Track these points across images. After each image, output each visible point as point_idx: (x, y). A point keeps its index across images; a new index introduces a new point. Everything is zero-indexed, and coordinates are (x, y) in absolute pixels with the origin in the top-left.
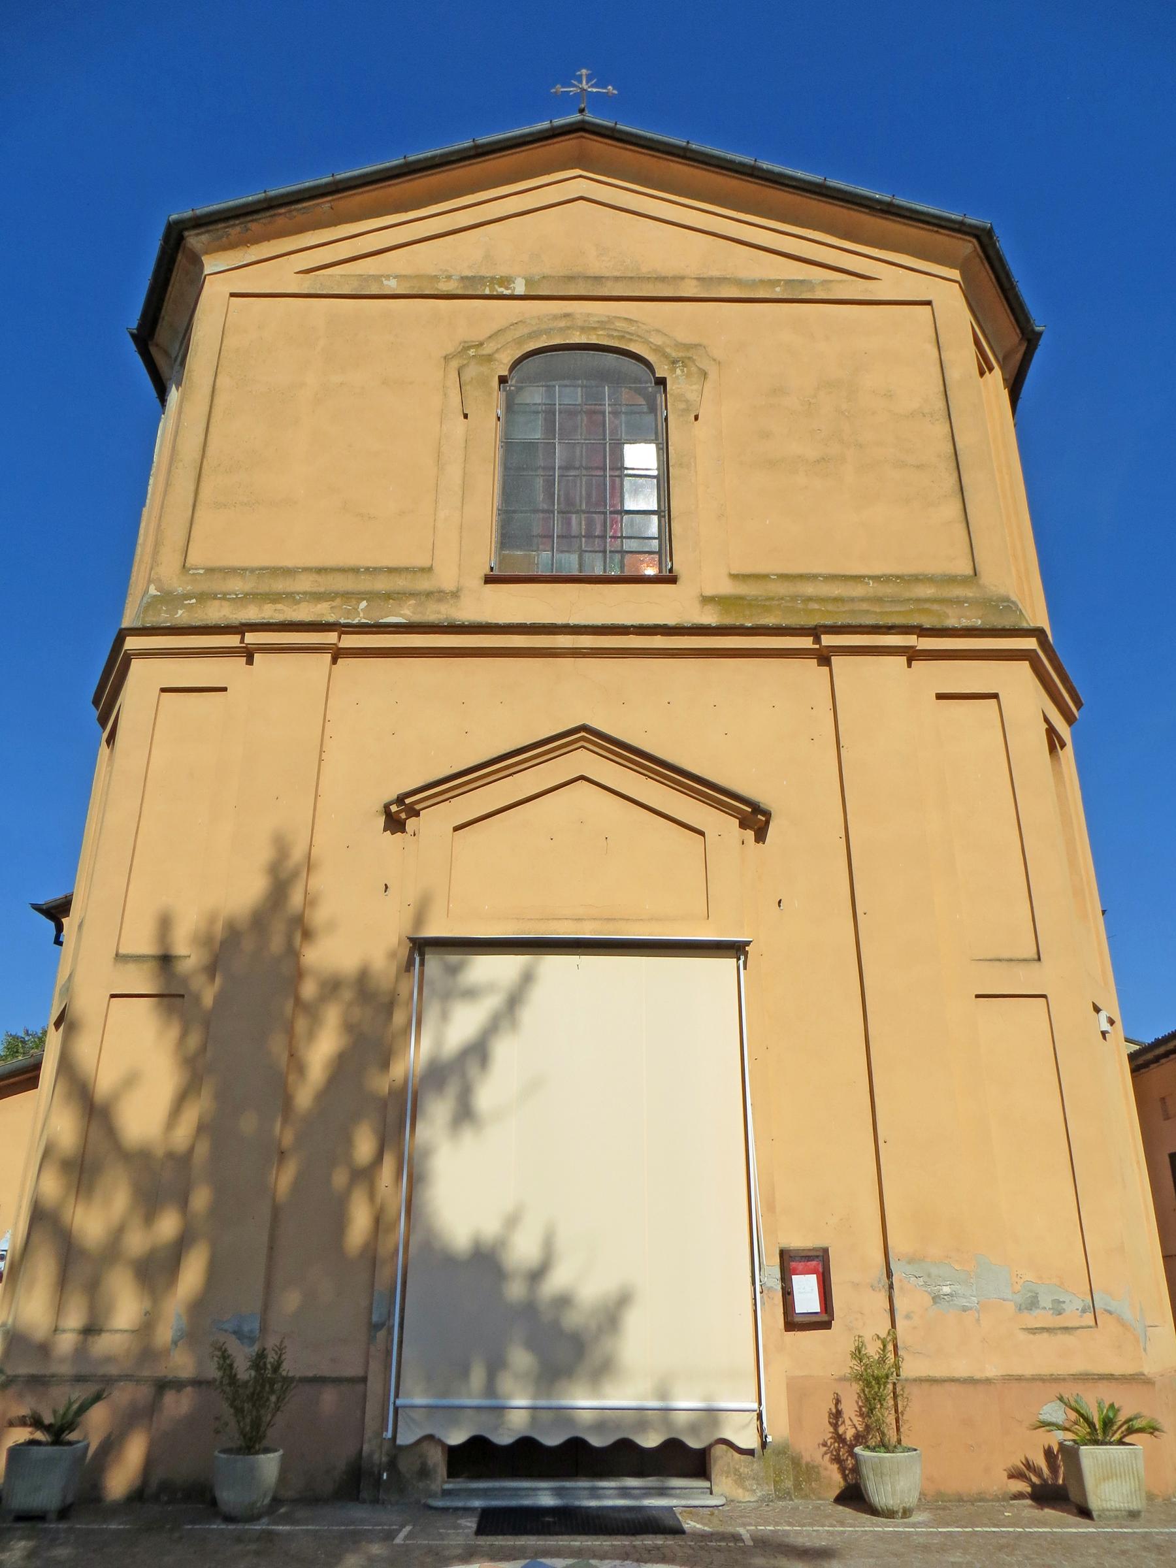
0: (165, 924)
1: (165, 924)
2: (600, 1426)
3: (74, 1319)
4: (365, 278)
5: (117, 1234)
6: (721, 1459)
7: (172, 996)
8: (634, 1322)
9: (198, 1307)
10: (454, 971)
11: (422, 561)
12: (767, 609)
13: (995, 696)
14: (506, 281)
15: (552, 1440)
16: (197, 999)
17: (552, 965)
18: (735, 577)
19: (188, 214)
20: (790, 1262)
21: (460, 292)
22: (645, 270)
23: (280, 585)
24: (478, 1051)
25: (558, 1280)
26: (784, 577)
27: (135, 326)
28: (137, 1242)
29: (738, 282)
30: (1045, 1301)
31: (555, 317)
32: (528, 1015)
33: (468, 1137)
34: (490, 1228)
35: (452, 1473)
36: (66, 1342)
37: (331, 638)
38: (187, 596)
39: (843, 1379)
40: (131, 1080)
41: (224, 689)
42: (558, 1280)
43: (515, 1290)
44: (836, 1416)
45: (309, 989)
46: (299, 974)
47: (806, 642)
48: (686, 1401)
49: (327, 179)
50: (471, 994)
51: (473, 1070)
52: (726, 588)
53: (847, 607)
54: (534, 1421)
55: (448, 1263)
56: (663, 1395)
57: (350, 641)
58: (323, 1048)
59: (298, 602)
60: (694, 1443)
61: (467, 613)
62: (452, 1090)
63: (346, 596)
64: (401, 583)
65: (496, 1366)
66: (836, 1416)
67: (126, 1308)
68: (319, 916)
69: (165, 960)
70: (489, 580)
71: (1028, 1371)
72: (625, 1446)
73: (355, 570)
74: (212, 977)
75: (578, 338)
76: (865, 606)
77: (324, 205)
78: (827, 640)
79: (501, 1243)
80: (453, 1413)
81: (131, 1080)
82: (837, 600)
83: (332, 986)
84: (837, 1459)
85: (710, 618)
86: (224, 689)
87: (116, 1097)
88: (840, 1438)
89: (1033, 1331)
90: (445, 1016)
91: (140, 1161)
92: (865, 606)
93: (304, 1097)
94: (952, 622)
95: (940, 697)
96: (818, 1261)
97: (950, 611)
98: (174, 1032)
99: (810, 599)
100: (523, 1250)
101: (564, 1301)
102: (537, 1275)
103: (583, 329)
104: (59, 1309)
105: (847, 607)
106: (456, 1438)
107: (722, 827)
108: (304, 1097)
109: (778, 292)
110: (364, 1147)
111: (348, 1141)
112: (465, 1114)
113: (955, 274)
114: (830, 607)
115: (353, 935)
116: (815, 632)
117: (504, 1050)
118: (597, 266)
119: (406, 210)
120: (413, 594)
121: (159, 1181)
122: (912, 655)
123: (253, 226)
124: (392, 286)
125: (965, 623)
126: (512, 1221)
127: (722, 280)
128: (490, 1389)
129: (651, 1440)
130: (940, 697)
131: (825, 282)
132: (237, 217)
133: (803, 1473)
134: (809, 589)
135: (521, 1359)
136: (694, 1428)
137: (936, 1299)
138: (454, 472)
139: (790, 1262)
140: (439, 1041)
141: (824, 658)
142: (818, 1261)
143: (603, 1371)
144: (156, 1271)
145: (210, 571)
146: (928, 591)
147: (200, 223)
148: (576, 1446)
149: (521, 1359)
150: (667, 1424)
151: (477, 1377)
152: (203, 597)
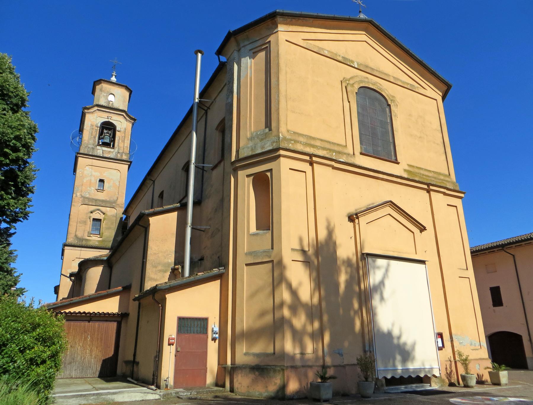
0: (301, 240)
1: (301, 240)
5: (304, 326)
6: (433, 379)
7: (307, 262)
9: (330, 345)
10: (374, 261)
12: (416, 176)
13: (305, 172)
14: (352, 62)
16: (313, 262)
17: (393, 262)
18: (408, 165)
19: (281, 11)
21: (342, 61)
22: (381, 69)
23: (312, 142)
24: (382, 283)
26: (417, 167)
27: (233, 30)
28: (309, 329)
29: (401, 81)
32: (390, 274)
34: (390, 327)
35: (387, 385)
36: (298, 356)
38: (291, 140)
39: (446, 361)
40: (300, 284)
42: (403, 340)
43: (395, 341)
44: (446, 368)
47: (426, 187)
48: (427, 366)
49: (315, 14)
50: (379, 268)
52: (407, 168)
54: (402, 372)
56: (423, 365)
58: (343, 278)
59: (319, 149)
62: (379, 293)
63: (330, 150)
65: (394, 359)
66: (446, 368)
67: (310, 348)
68: (338, 243)
69: (304, 252)
72: (418, 377)
74: (321, 258)
76: (433, 179)
78: (431, 187)
80: (387, 371)
81: (300, 284)
83: (344, 262)
84: (447, 378)
85: (405, 175)
88: (447, 373)
89: (473, 350)
90: (374, 273)
91: (305, 306)
92: (433, 179)
95: (448, 205)
98: (308, 272)
99: (423, 175)
100: (396, 332)
101: (405, 344)
102: (399, 338)
104: (294, 347)
106: (389, 377)
109: (409, 87)
110: (356, 305)
111: (352, 304)
112: (382, 298)
115: (345, 250)
116: (428, 185)
118: (371, 65)
121: (313, 313)
122: (445, 194)
123: (294, 20)
124: (326, 53)
126: (393, 325)
128: (394, 365)
130: (448, 205)
131: (417, 87)
132: (291, 16)
133: (443, 381)
134: (422, 172)
135: (398, 358)
137: (460, 343)
140: (374, 280)
141: (428, 191)
143: (413, 359)
144: (317, 336)
145: (295, 133)
147: (283, 15)
149: (398, 358)
152: (296, 142)
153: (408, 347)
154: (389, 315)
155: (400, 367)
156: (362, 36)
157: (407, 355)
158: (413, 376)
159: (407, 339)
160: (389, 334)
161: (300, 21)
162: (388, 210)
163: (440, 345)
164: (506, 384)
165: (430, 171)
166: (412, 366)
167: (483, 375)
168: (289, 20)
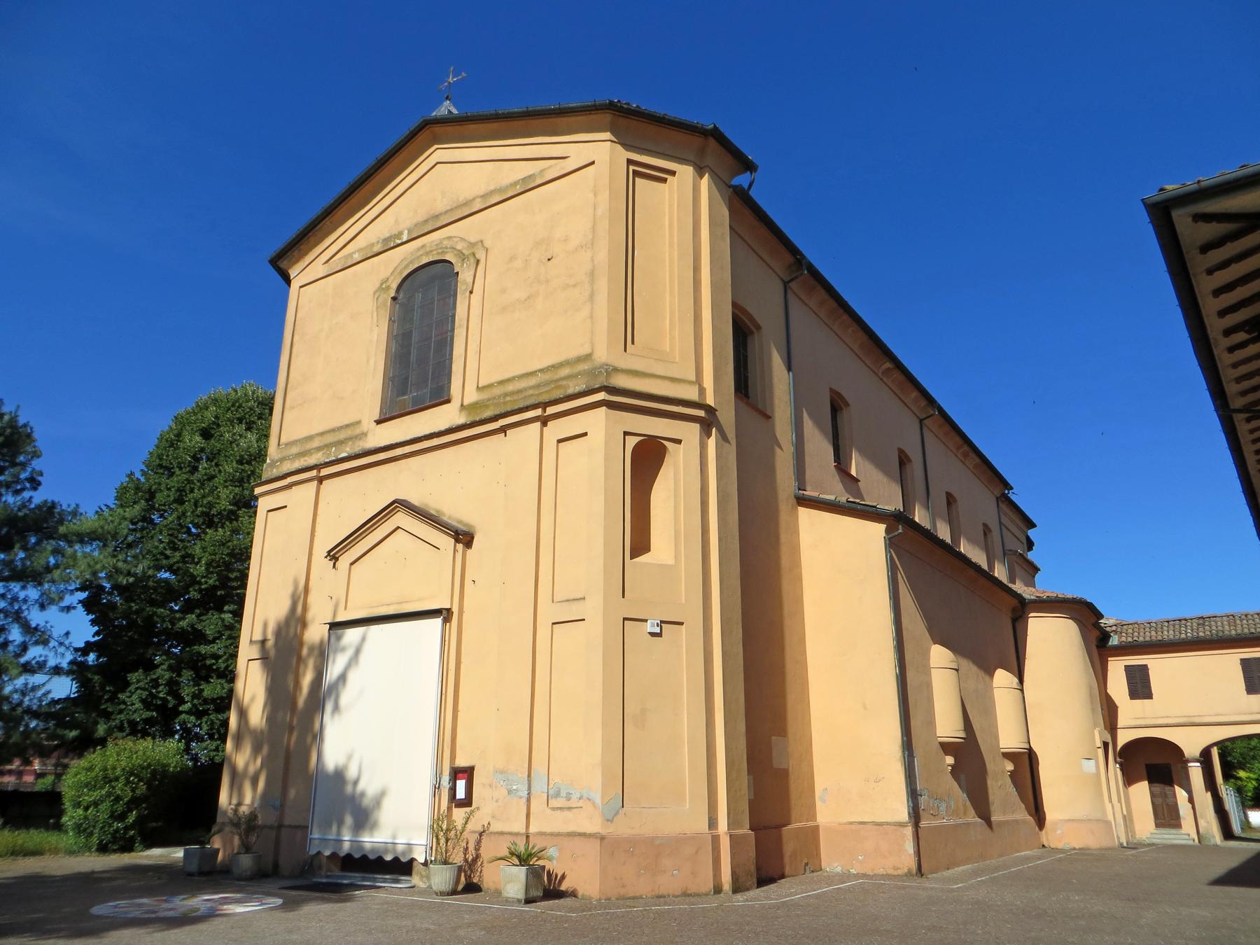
2: (373, 850)
3: (234, 801)
4: (346, 257)
8: (387, 804)
11: (585, 350)
12: (487, 407)
15: (357, 856)
20: (456, 773)
24: (343, 678)
25: (361, 786)
30: (563, 793)
31: (419, 249)
32: (363, 657)
33: (336, 717)
37: (314, 473)
40: (253, 699)
41: (585, 434)
43: (349, 789)
45: (305, 651)
46: (301, 644)
51: (340, 686)
53: (521, 396)
55: (327, 776)
57: (324, 472)
60: (404, 860)
61: (371, 443)
64: (349, 433)
65: (341, 823)
70: (378, 422)
71: (548, 830)
73: (333, 430)
75: (425, 260)
77: (327, 221)
79: (345, 767)
81: (253, 699)
82: (520, 391)
83: (311, 649)
86: (585, 434)
87: (248, 707)
92: (531, 392)
93: (301, 701)
94: (570, 391)
96: (467, 773)
97: (571, 384)
100: (352, 773)
101: (363, 794)
102: (356, 783)
103: (427, 254)
105: (521, 396)
107: (446, 542)
108: (301, 701)
109: (519, 189)
112: (336, 708)
113: (607, 135)
114: (515, 397)
117: (352, 677)
118: (441, 206)
119: (364, 206)
120: (350, 439)
124: (357, 257)
125: (577, 389)
126: (350, 757)
127: (492, 193)
128: (339, 833)
129: (389, 858)
135: (349, 820)
136: (404, 853)
137: (510, 792)
138: (372, 361)
139: (456, 773)
142: (467, 773)
143: (374, 826)
146: (565, 372)
148: (364, 857)
149: (349, 820)
150: (394, 850)
151: (334, 828)
153: (366, 802)
154: (342, 743)
155: (347, 837)
156: (439, 153)
157: (363, 817)
158: (372, 857)
159: (368, 787)
160: (339, 775)
161: (312, 239)
162: (401, 519)
163: (461, 794)
164: (519, 901)
165: (533, 374)
166: (373, 840)
167: (563, 877)
168: (296, 253)
